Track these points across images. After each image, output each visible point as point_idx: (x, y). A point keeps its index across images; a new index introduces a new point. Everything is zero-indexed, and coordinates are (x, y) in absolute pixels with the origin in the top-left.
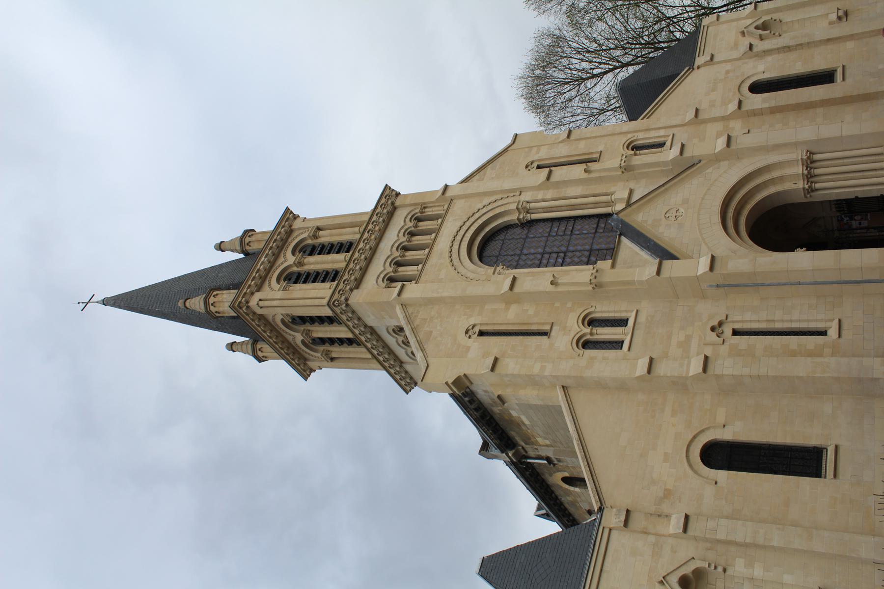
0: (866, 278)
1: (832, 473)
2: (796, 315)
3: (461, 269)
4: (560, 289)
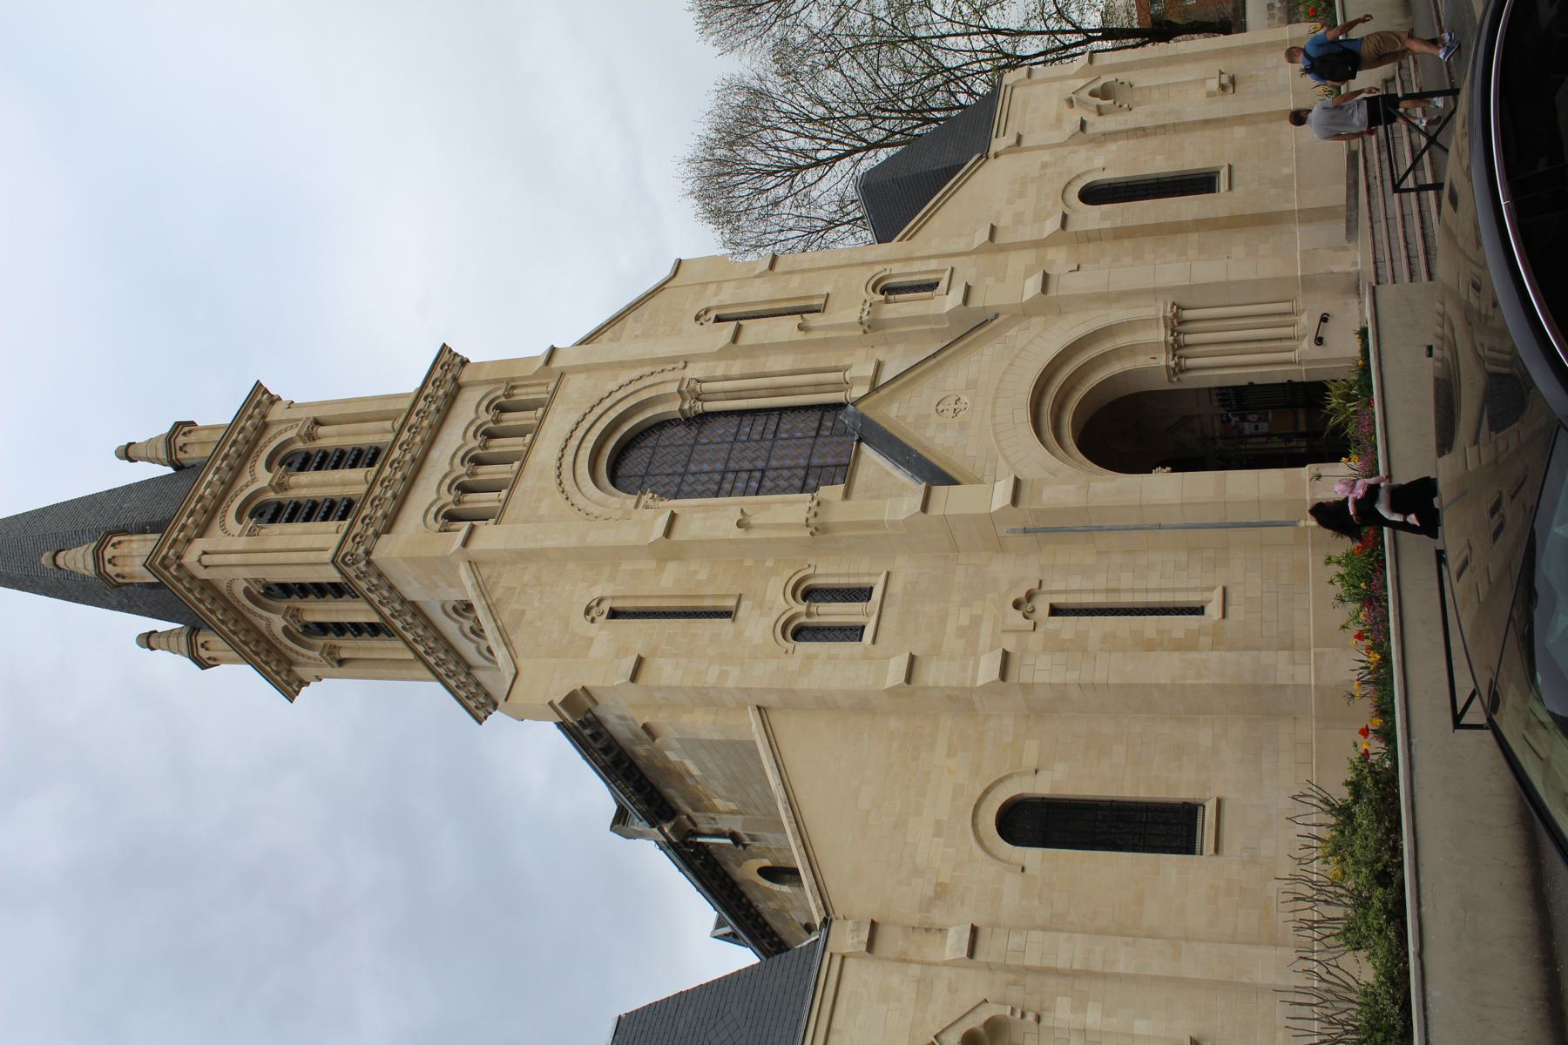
0: (1265, 518)
1: (1212, 846)
2: (1154, 581)
3: (577, 498)
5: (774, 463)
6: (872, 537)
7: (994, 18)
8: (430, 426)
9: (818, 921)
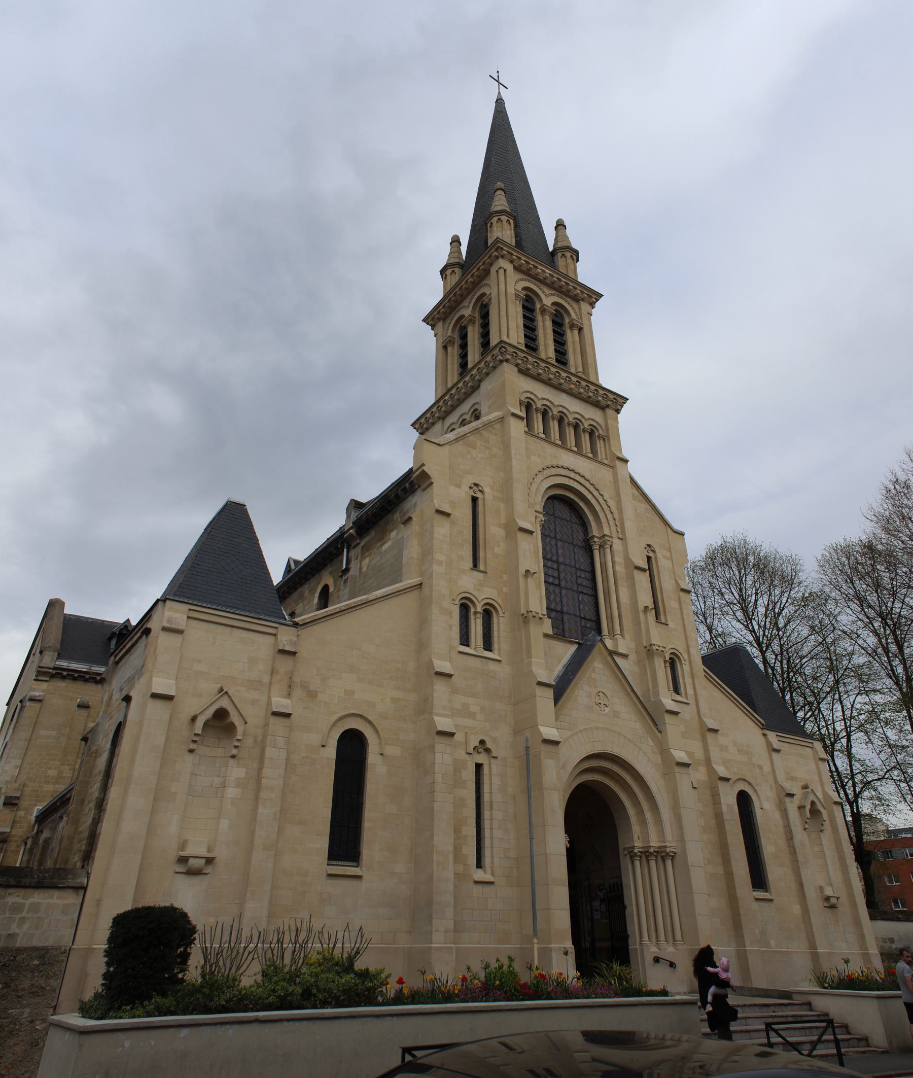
0: (538, 914)
1: (333, 872)
2: (497, 834)
3: (540, 477)
4: (522, 580)
5: (564, 592)
6: (522, 651)
7: (858, 737)
8: (580, 393)
9: (296, 620)
